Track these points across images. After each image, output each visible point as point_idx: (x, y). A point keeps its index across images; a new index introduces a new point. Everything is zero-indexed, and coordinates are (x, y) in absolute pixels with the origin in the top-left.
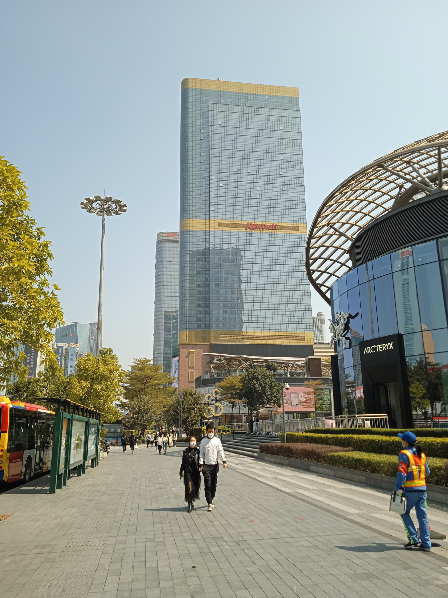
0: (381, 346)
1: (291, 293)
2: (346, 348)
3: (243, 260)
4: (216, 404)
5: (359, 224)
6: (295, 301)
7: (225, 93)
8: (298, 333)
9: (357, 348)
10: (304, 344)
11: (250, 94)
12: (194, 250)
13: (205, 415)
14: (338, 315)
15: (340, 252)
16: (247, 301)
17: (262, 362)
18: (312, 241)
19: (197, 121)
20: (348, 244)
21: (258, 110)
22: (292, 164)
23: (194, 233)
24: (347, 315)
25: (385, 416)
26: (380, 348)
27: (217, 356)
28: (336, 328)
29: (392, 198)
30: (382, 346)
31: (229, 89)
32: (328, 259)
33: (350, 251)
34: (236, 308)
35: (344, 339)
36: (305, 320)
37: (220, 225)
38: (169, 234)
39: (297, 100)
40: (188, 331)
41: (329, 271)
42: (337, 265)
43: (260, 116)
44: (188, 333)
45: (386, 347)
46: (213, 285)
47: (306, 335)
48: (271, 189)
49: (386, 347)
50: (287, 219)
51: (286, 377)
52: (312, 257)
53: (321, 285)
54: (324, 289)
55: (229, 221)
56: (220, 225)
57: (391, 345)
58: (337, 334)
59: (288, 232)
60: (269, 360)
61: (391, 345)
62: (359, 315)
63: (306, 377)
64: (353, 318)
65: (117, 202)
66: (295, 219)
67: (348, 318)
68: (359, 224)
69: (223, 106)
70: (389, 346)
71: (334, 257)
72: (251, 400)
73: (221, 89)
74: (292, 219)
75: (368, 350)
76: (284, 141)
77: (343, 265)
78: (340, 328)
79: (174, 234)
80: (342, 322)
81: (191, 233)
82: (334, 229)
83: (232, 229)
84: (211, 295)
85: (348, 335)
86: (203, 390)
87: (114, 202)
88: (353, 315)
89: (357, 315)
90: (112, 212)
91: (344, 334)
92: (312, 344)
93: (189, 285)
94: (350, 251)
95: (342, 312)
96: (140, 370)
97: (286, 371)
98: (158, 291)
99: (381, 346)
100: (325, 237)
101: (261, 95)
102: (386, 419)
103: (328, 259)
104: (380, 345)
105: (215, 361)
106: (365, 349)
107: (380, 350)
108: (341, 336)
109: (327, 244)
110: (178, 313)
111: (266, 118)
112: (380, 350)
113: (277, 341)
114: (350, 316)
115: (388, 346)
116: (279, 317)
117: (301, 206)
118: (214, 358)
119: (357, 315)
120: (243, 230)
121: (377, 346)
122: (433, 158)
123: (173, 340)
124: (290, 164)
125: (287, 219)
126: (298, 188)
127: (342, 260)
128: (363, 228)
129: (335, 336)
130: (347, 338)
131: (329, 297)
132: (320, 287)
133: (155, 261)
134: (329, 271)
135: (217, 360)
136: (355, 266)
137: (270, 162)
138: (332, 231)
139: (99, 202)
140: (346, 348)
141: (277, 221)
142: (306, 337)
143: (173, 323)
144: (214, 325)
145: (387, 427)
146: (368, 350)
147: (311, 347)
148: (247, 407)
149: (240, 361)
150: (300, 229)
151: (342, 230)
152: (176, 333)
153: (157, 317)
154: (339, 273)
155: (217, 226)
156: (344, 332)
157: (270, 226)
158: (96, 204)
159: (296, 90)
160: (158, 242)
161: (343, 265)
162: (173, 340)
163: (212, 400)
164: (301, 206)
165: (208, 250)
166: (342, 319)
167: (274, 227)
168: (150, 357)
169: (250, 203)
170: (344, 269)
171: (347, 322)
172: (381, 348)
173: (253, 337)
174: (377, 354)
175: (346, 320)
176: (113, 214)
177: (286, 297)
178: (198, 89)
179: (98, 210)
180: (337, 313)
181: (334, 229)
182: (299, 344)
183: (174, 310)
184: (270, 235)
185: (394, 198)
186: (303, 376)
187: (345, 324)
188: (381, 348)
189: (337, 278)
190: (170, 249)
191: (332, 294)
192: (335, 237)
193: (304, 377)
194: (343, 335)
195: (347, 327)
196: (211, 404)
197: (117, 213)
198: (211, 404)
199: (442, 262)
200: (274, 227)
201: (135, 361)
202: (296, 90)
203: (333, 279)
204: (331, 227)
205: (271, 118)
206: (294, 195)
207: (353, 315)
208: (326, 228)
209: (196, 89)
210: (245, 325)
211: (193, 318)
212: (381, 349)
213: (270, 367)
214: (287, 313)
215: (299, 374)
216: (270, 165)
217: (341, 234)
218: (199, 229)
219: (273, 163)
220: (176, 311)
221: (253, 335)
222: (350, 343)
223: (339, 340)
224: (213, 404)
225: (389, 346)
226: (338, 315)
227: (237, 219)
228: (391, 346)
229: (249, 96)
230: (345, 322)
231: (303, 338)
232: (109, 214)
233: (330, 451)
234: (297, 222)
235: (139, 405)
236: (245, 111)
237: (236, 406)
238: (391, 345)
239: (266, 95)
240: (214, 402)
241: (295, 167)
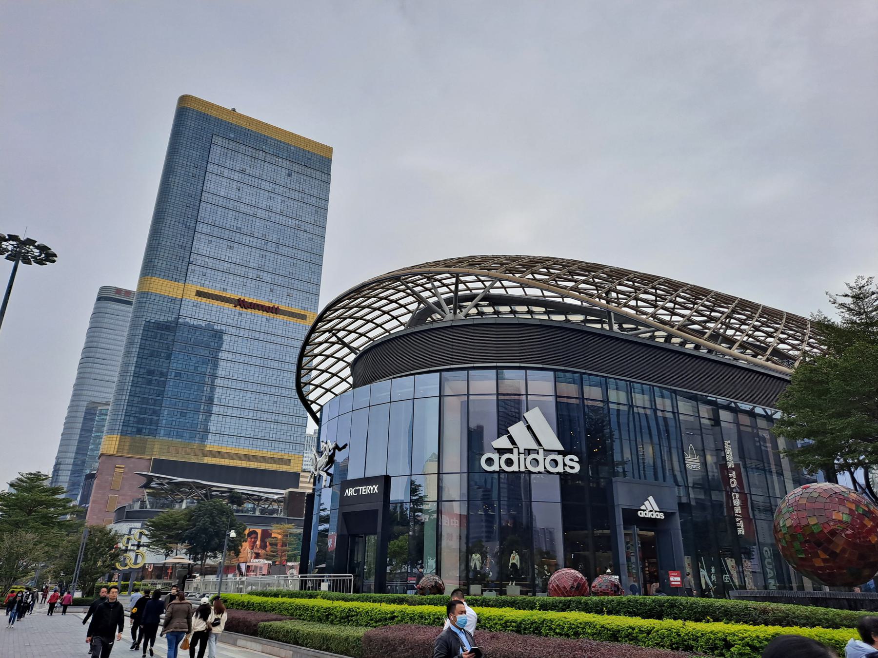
0: (365, 489)
1: (282, 400)
2: (325, 487)
3: (224, 346)
4: (137, 551)
5: (369, 335)
6: (286, 411)
7: (237, 128)
8: (283, 454)
9: (337, 489)
10: (288, 470)
11: (271, 139)
12: (153, 321)
13: (118, 565)
14: (324, 443)
15: (341, 364)
16: (219, 403)
17: (226, 492)
18: (308, 348)
19: (191, 151)
20: (351, 358)
21: (277, 159)
22: (311, 236)
23: (157, 298)
24: (334, 445)
25: (351, 576)
26: (363, 490)
27: (158, 478)
28: (318, 459)
29: (410, 312)
30: (365, 489)
31: (244, 124)
32: (326, 371)
33: (353, 365)
34: (202, 411)
35: (324, 474)
36: (295, 438)
37: (199, 294)
38: (118, 291)
39: (330, 161)
40: (119, 436)
41: (325, 385)
42: (336, 380)
43: (279, 169)
44: (118, 439)
45: (370, 490)
46: (173, 374)
47: (293, 458)
48: (279, 260)
49: (370, 490)
50: (294, 303)
51: (254, 515)
52: (305, 367)
53: (313, 402)
54: (315, 407)
55: (214, 290)
56: (199, 294)
57: (374, 489)
58: (318, 467)
59: (292, 320)
60: (234, 489)
61: (374, 489)
62: (347, 447)
63: (281, 516)
64: (340, 450)
65: (43, 249)
66: (303, 305)
67: (334, 449)
68: (369, 335)
69: (231, 143)
70: (374, 489)
71: (333, 370)
72: (197, 546)
73: (234, 121)
74: (300, 304)
75: (350, 492)
76: (305, 205)
77: (343, 380)
78: (323, 460)
79: (128, 293)
80: (327, 453)
81: (153, 297)
82: (337, 337)
83: (216, 303)
84: (167, 389)
85: (331, 471)
86: (123, 528)
87: (37, 247)
88: (341, 446)
89: (345, 447)
90: (32, 260)
91: (326, 468)
92: (299, 470)
93: (118, 446)
94: (353, 365)
95: (329, 441)
96: (29, 489)
97: (256, 506)
98: (91, 345)
99: (365, 489)
100: (325, 345)
101: (284, 143)
102: (351, 580)
103: (326, 371)
104: (363, 487)
105: (153, 485)
106: (347, 491)
107: (363, 493)
108: (322, 470)
109: (327, 353)
110: (110, 408)
111: (287, 172)
112: (363, 493)
113: (252, 463)
114: (337, 447)
115: (372, 489)
116: (261, 431)
117: (314, 290)
118: (152, 481)
119: (345, 447)
120: (231, 306)
121: (360, 488)
122: (325, 374)
123: (93, 446)
124: (308, 235)
125: (294, 303)
126: (313, 267)
127: (343, 374)
128: (373, 340)
129: (316, 470)
130: (329, 474)
131: (319, 416)
132: (311, 404)
133: (87, 325)
134: (338, 380)
135: (156, 484)
136: (354, 386)
137: (283, 227)
138: (334, 339)
139: (14, 243)
140: (325, 487)
141: (280, 303)
142: (292, 461)
143: (99, 421)
144: (162, 432)
145: (350, 592)
146: (350, 492)
147: (297, 475)
148: (188, 555)
149: (191, 488)
150: (307, 319)
151: (346, 340)
152: (100, 437)
153: (73, 409)
154: (337, 390)
155: (194, 294)
156: (326, 466)
157: (269, 307)
158: (8, 244)
159: (330, 150)
160: (99, 299)
161: (343, 380)
162: (93, 446)
163: (133, 545)
164: (314, 290)
165: (175, 325)
166: (327, 450)
167: (275, 310)
168: (47, 470)
169: (246, 273)
170: (345, 386)
171: (332, 454)
172: (365, 490)
173: (219, 454)
174: (359, 497)
175: (332, 451)
176: (33, 262)
177: (275, 405)
178: (201, 113)
179: (10, 253)
180: (323, 442)
181: (337, 337)
182: (281, 469)
183: (104, 401)
184: (268, 320)
185: (412, 312)
186: (277, 514)
187: (329, 456)
188: (365, 490)
189: (334, 396)
190: (116, 312)
191: (321, 415)
192: (337, 346)
193: (279, 516)
194: (325, 470)
195: (331, 460)
196: (131, 550)
197: (40, 262)
198: (131, 550)
199: (442, 397)
200: (275, 310)
201: (20, 476)
202: (330, 150)
203: (329, 396)
204: (334, 335)
205: (293, 174)
206: (306, 275)
207: (341, 446)
208: (327, 335)
209: (197, 112)
210: (210, 437)
211: (132, 419)
212: (365, 492)
213: (236, 499)
214: (272, 425)
215: (275, 511)
216: (283, 231)
217: (345, 345)
218: (166, 294)
219: (286, 229)
220: (108, 404)
221: (219, 452)
222: (331, 481)
223: (320, 475)
224: (134, 551)
225: (374, 489)
226: (324, 443)
227: (224, 290)
228: (376, 490)
229: (269, 140)
230: (330, 454)
231: (288, 462)
232: (27, 262)
233: (262, 621)
234: (306, 309)
235: (10, 546)
236: (261, 156)
237: (172, 552)
238: (376, 488)
239: (291, 145)
240: (135, 548)
241: (314, 240)
